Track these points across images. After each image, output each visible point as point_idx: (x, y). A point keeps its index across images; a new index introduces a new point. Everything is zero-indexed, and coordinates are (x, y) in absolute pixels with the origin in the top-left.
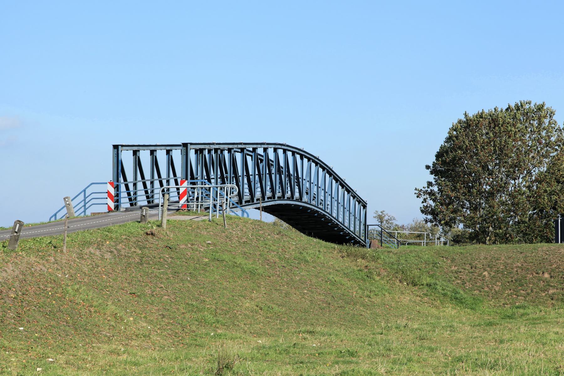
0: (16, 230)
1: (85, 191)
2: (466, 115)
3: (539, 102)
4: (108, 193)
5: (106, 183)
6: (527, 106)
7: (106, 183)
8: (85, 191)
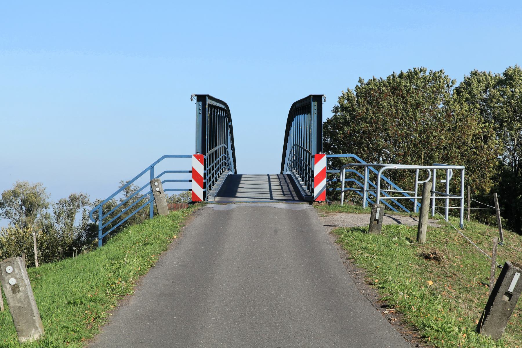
0: (511, 289)
1: (152, 168)
2: (360, 81)
3: (436, 69)
4: (193, 172)
5: (190, 156)
6: (421, 74)
7: (190, 156)
8: (152, 168)
